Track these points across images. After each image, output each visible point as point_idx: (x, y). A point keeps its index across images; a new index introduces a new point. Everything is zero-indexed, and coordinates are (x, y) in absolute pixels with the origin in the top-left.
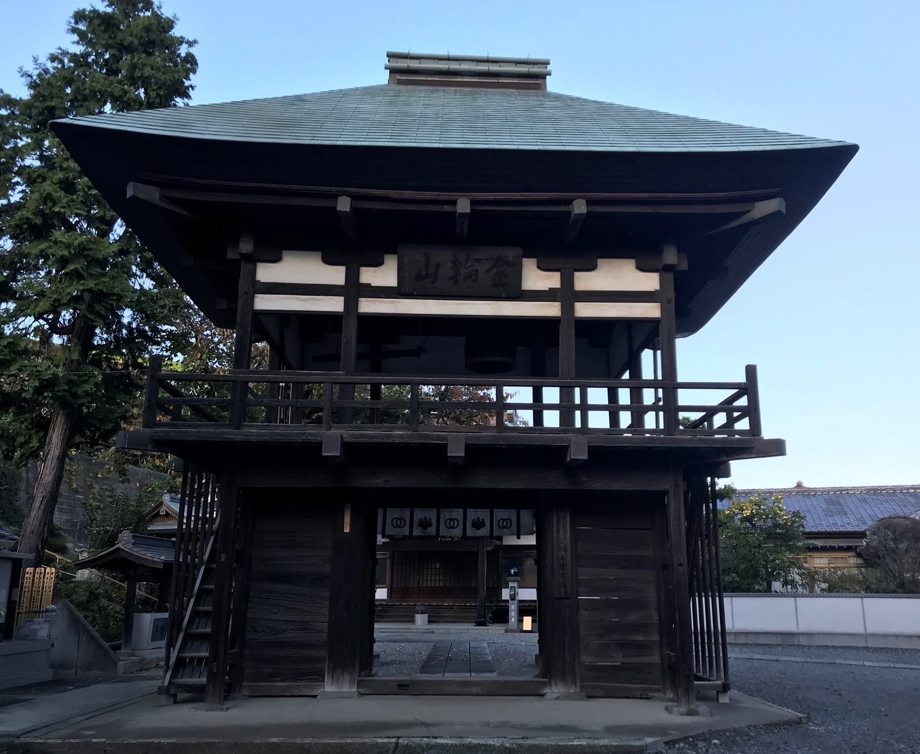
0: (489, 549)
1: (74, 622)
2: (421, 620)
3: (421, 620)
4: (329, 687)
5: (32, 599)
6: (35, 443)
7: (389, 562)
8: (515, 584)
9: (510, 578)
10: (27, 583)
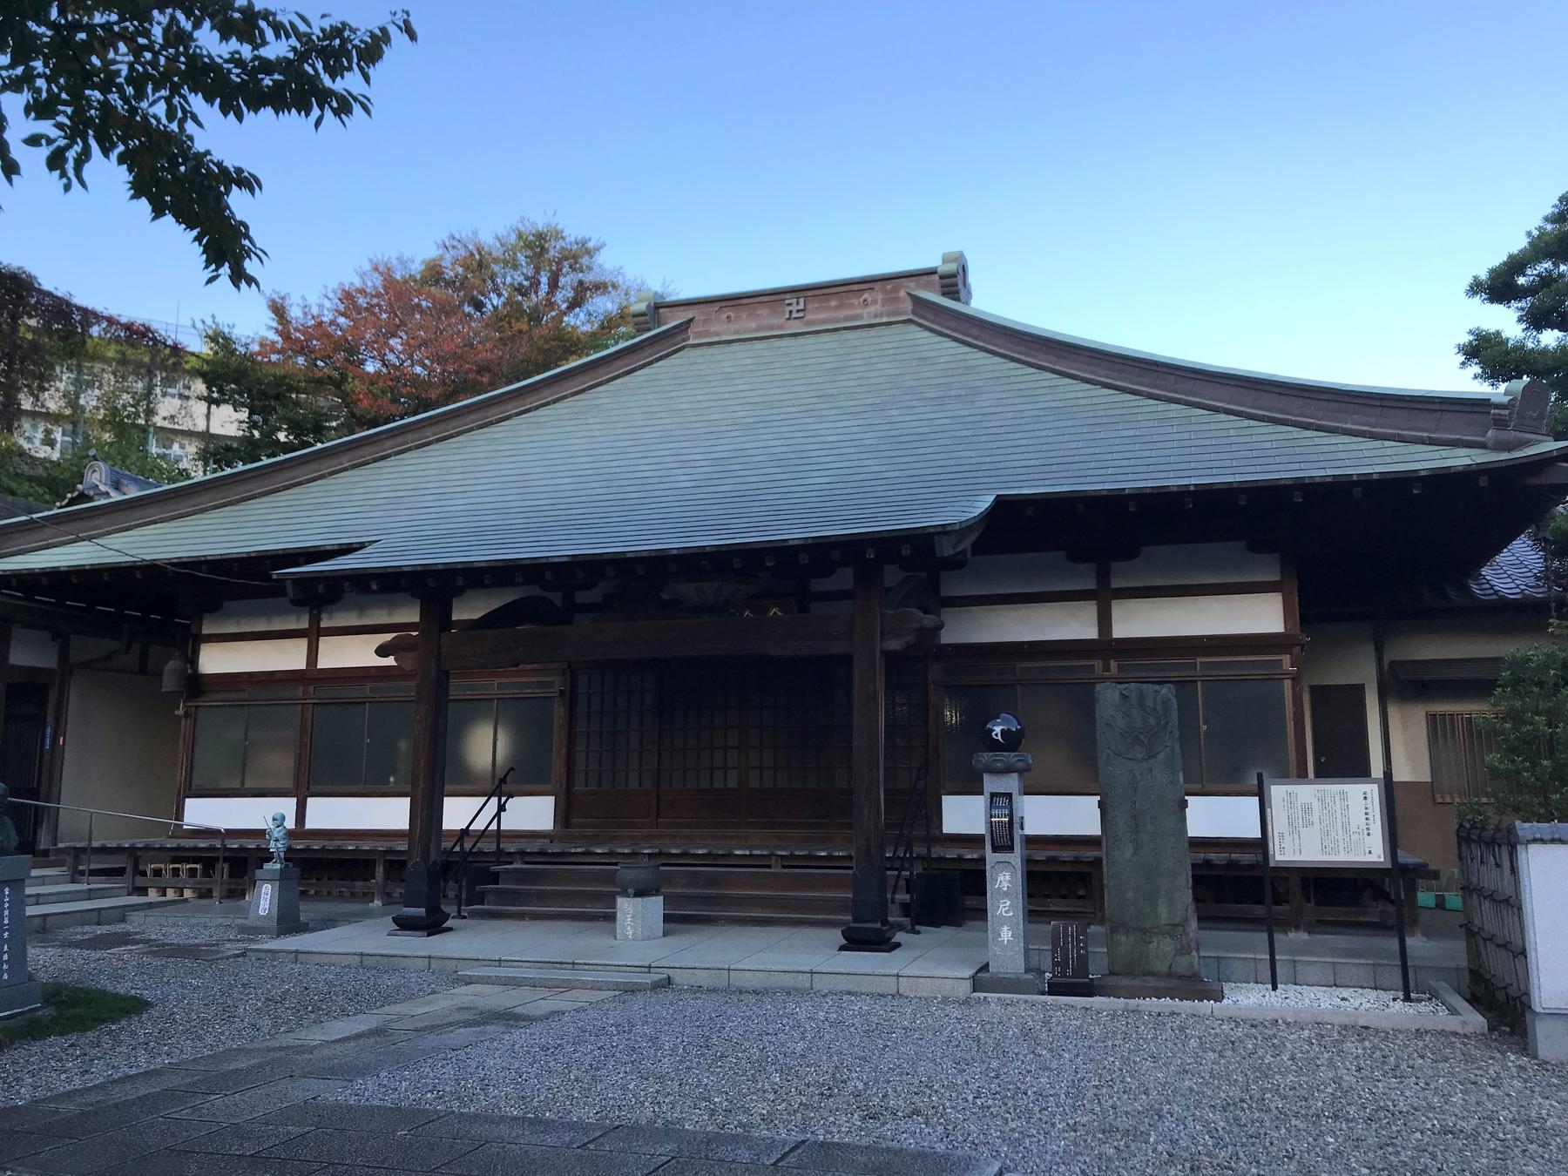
0: (894, 645)
2: (637, 915)
3: (637, 915)
7: (559, 711)
8: (1010, 783)
9: (986, 757)
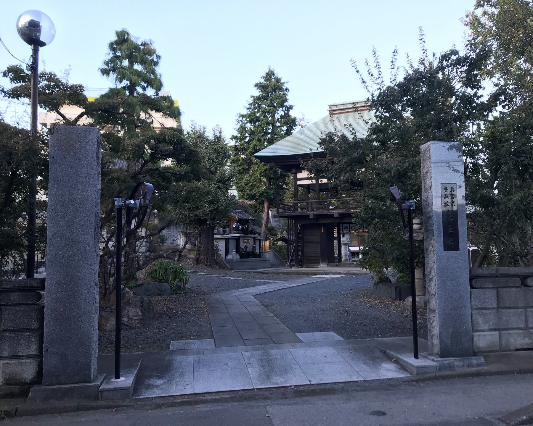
1: (275, 254)
4: (321, 265)
5: (265, 249)
6: (261, 209)
10: (263, 245)
